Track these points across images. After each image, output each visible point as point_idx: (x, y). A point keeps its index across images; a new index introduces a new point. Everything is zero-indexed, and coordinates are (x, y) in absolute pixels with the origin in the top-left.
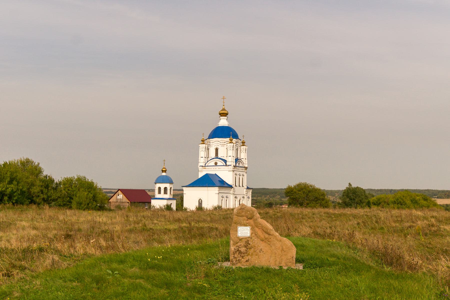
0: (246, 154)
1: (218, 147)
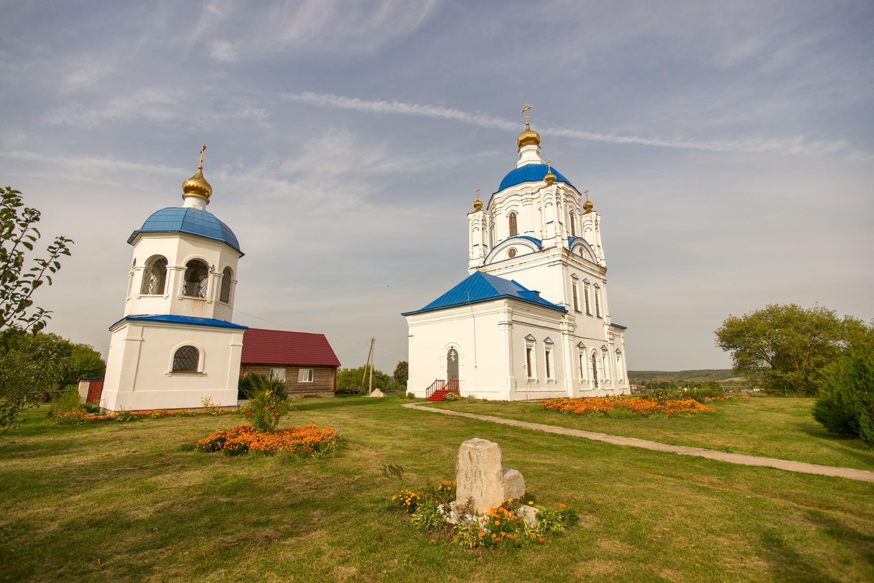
0: (599, 235)
1: (514, 208)
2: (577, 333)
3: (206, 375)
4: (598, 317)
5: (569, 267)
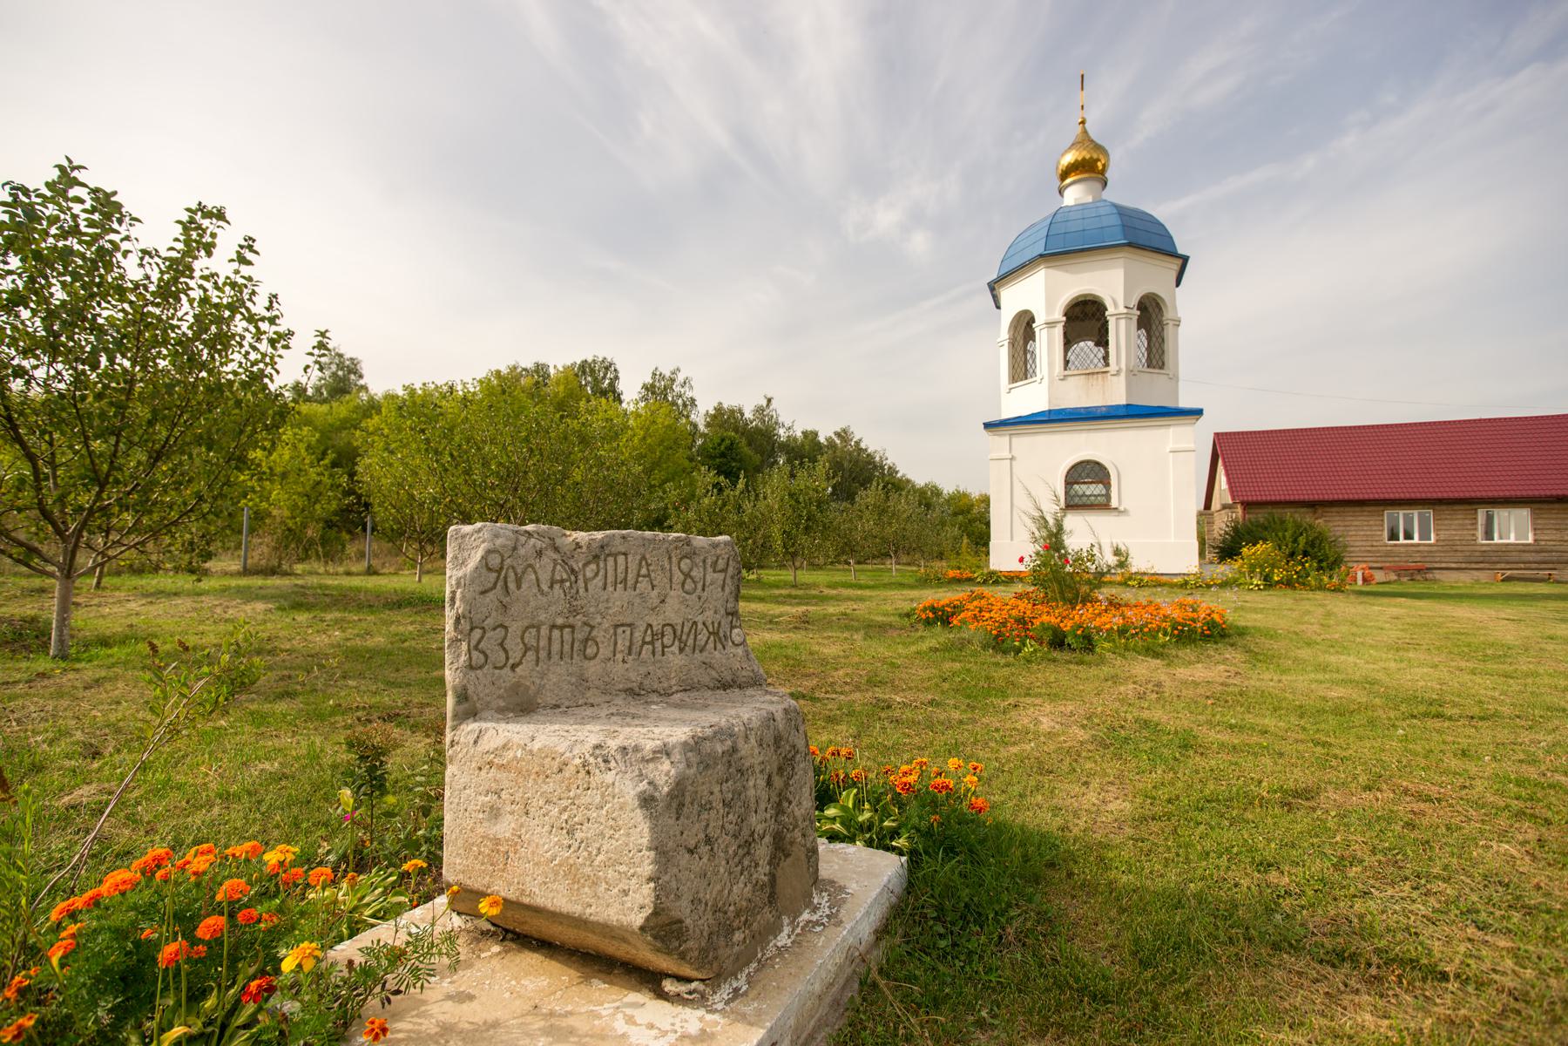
3: (1125, 512)
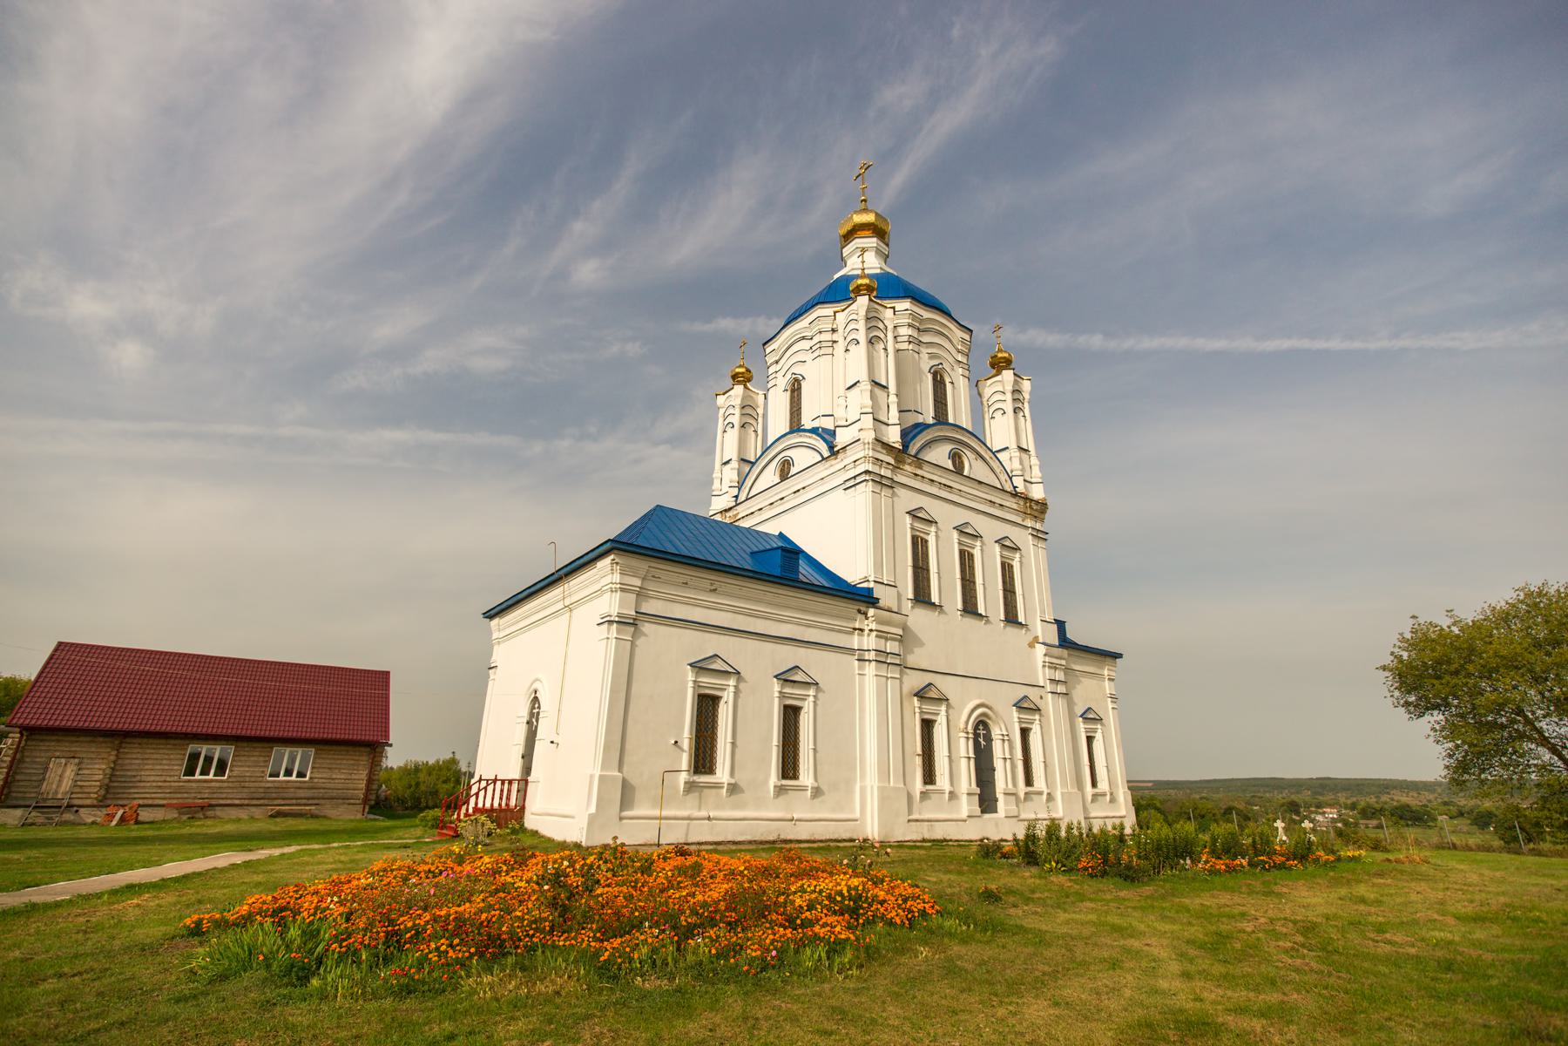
1: (798, 369)
2: (912, 660)
4: (1011, 618)
5: (901, 491)
